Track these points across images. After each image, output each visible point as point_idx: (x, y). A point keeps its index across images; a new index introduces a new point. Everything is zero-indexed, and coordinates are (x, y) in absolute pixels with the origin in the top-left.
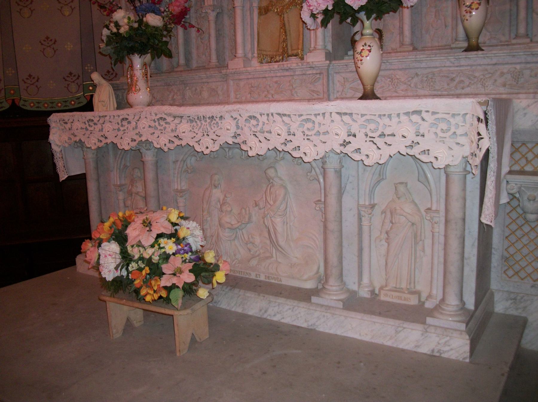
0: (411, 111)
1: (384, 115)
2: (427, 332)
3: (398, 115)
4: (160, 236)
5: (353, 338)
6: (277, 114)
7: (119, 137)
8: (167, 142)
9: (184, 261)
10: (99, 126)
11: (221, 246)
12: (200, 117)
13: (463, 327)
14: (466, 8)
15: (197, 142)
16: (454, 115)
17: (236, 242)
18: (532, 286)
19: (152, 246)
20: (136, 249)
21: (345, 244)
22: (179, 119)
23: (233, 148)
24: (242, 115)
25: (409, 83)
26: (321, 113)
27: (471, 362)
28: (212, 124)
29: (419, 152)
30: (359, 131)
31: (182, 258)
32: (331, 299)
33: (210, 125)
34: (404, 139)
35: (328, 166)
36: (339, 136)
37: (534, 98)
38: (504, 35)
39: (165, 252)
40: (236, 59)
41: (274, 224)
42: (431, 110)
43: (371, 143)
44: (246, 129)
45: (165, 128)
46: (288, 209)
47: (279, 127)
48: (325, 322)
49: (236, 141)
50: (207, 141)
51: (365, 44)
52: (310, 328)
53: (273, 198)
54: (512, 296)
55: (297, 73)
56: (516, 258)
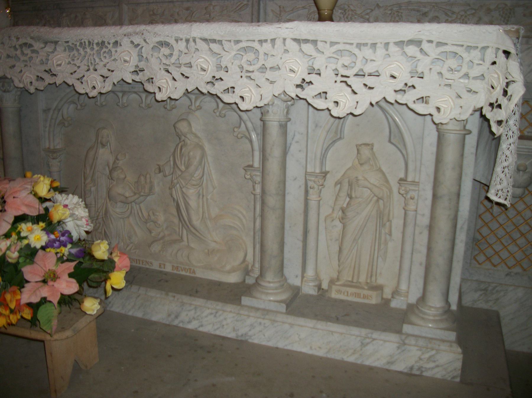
0: (406, 39)
2: (405, 344)
3: (387, 44)
4: (20, 219)
5: (301, 353)
6: (201, 39)
8: (33, 78)
9: (61, 260)
11: (111, 226)
12: (84, 43)
15: (78, 79)
17: (131, 219)
18: (507, 275)
22: (53, 46)
23: (129, 92)
24: (147, 40)
25: (367, 17)
26: (269, 38)
27: (461, 381)
28: (102, 53)
29: (415, 99)
30: (326, 66)
31: (57, 253)
32: (270, 301)
34: (392, 81)
36: (295, 74)
39: (28, 245)
41: (185, 197)
43: (344, 84)
45: (31, 58)
46: (205, 176)
47: (203, 58)
48: (261, 331)
49: (137, 79)
52: (239, 338)
53: (185, 160)
54: (482, 286)
56: (489, 241)
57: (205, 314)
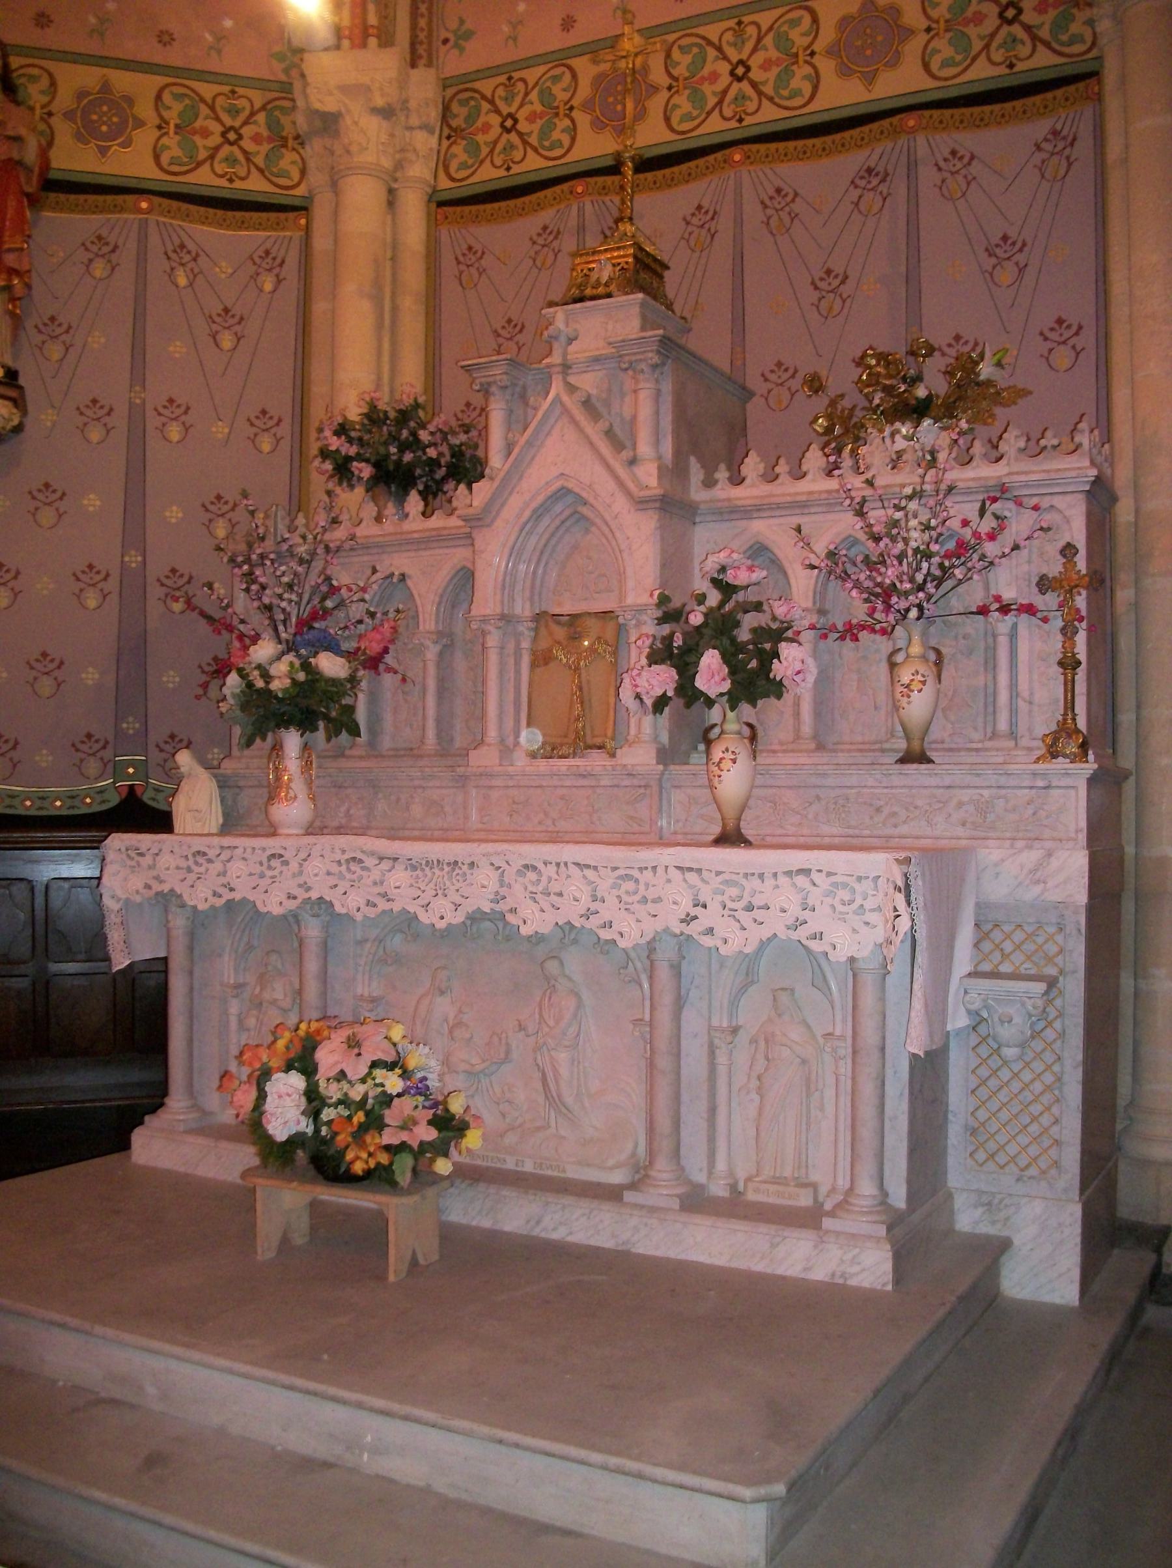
1: (753, 874)
3: (775, 875)
7: (261, 889)
10: (218, 866)
13: (882, 1230)
14: (902, 689)
16: (859, 879)
18: (1018, 1180)
19: (363, 1081)
20: (334, 1086)
21: (685, 1097)
26: (650, 865)
32: (662, 1195)
33: (450, 878)
35: (658, 955)
37: (1012, 846)
38: (975, 729)
40: (486, 748)
42: (825, 869)
44: (518, 888)
45: (361, 878)
49: (497, 908)
50: (442, 905)
51: (727, 750)
54: (985, 1199)
55: (603, 783)
57: (574, 1217)
